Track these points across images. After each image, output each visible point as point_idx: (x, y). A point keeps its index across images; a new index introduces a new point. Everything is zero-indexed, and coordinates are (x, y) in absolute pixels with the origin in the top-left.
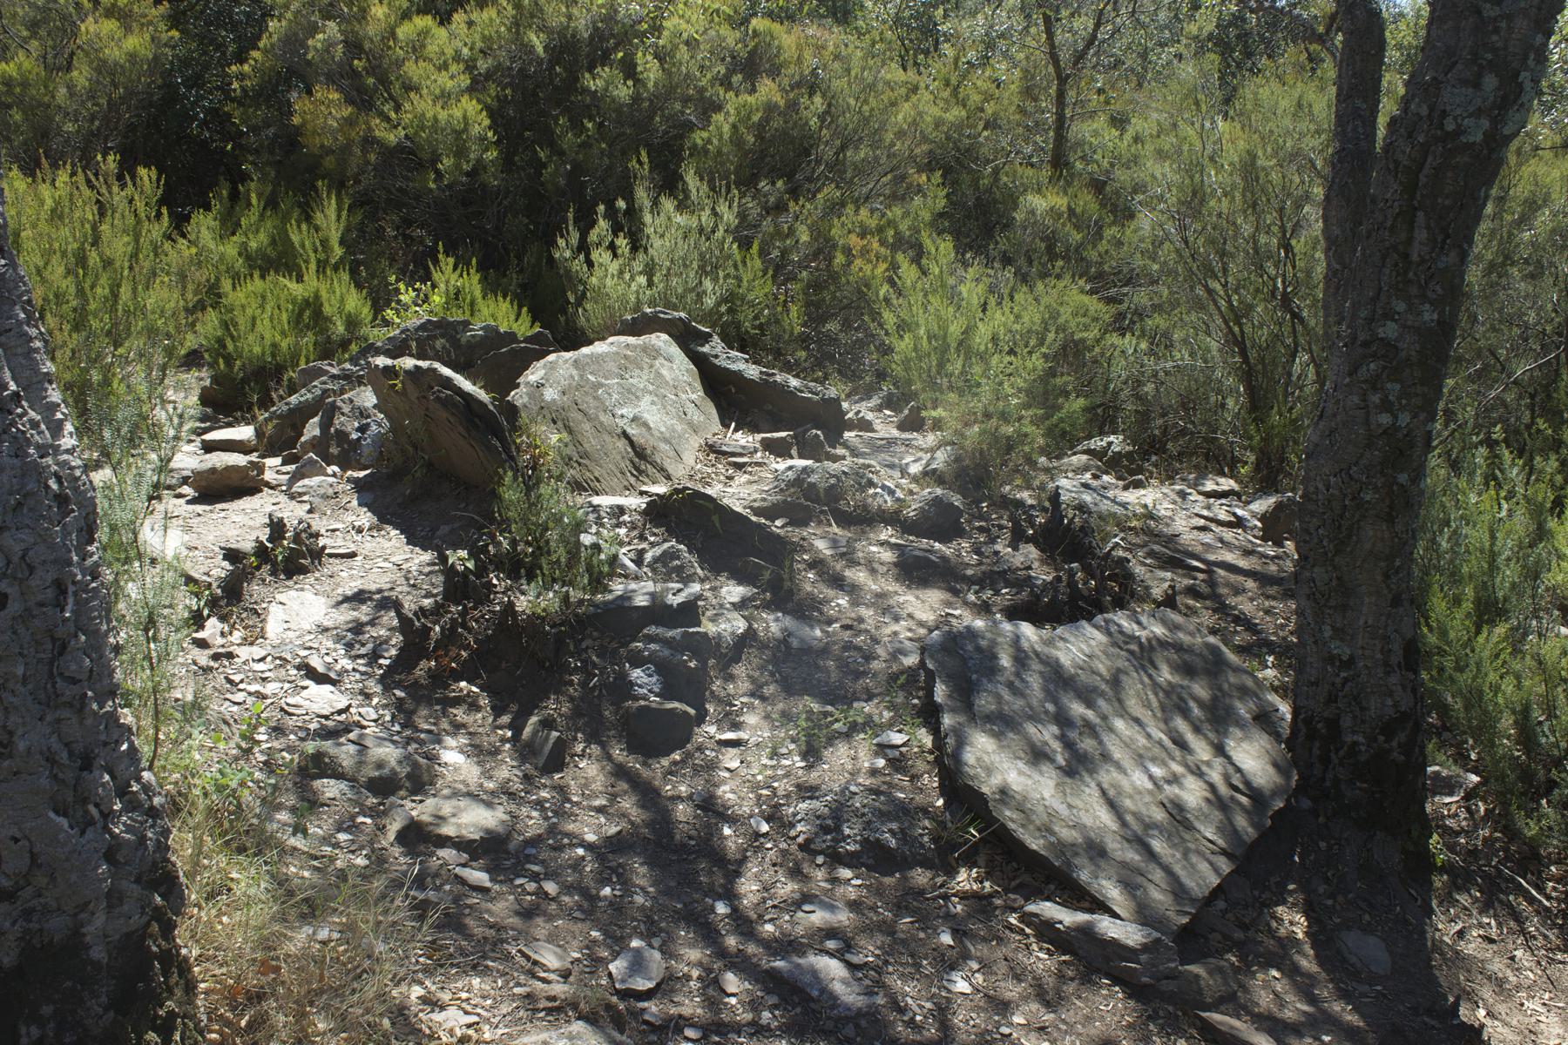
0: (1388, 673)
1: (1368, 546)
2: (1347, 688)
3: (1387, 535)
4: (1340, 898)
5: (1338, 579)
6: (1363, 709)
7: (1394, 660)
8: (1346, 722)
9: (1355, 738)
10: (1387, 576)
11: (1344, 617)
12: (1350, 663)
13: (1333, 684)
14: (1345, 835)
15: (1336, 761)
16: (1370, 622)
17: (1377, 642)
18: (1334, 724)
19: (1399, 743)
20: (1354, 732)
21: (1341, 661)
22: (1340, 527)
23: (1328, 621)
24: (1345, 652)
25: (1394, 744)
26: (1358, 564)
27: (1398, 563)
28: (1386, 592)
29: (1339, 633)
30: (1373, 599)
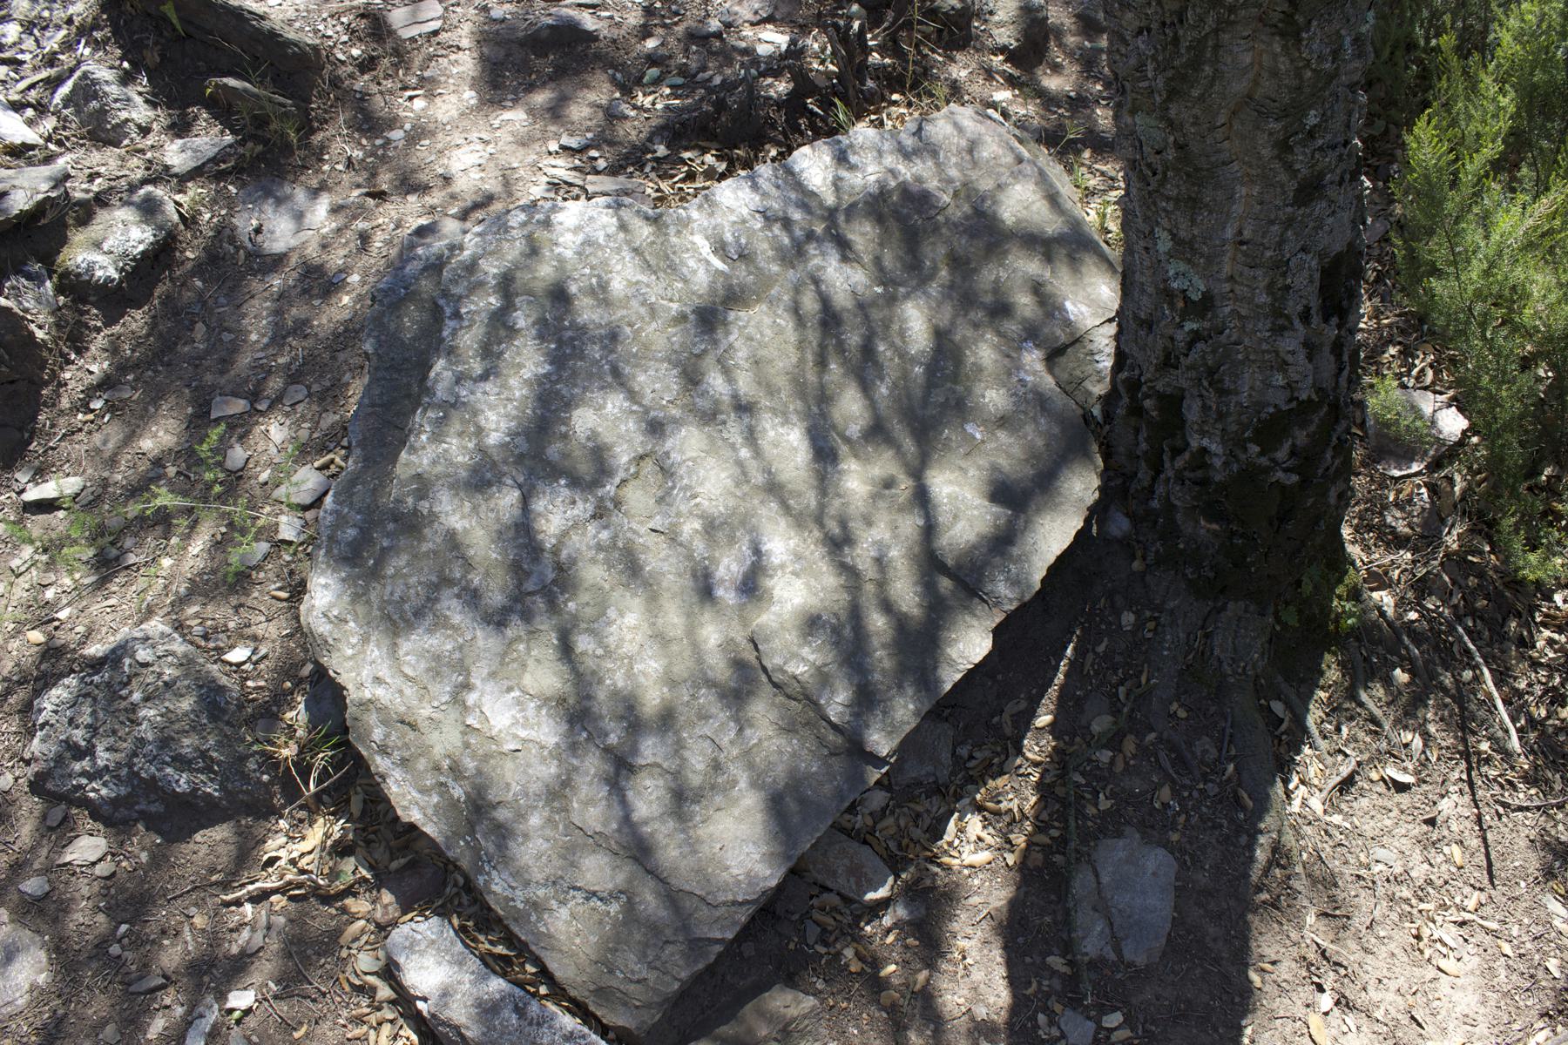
0: (1278, 330)
1: (1239, 87)
2: (1194, 356)
3: (1283, 64)
4: (1130, 745)
5: (1180, 147)
6: (1223, 392)
7: (1293, 307)
8: (1192, 411)
9: (1205, 442)
10: (1284, 147)
11: (1193, 221)
12: (1206, 305)
13: (1172, 339)
14: (1171, 604)
15: (1170, 473)
16: (1247, 234)
17: (1259, 272)
18: (1172, 403)
19: (1293, 453)
20: (1203, 433)
21: (1186, 299)
22: (1176, 40)
23: (1165, 222)
24: (1197, 287)
25: (1281, 454)
26: (1221, 120)
27: (1312, 119)
28: (1283, 177)
29: (1184, 248)
30: (1256, 190)
